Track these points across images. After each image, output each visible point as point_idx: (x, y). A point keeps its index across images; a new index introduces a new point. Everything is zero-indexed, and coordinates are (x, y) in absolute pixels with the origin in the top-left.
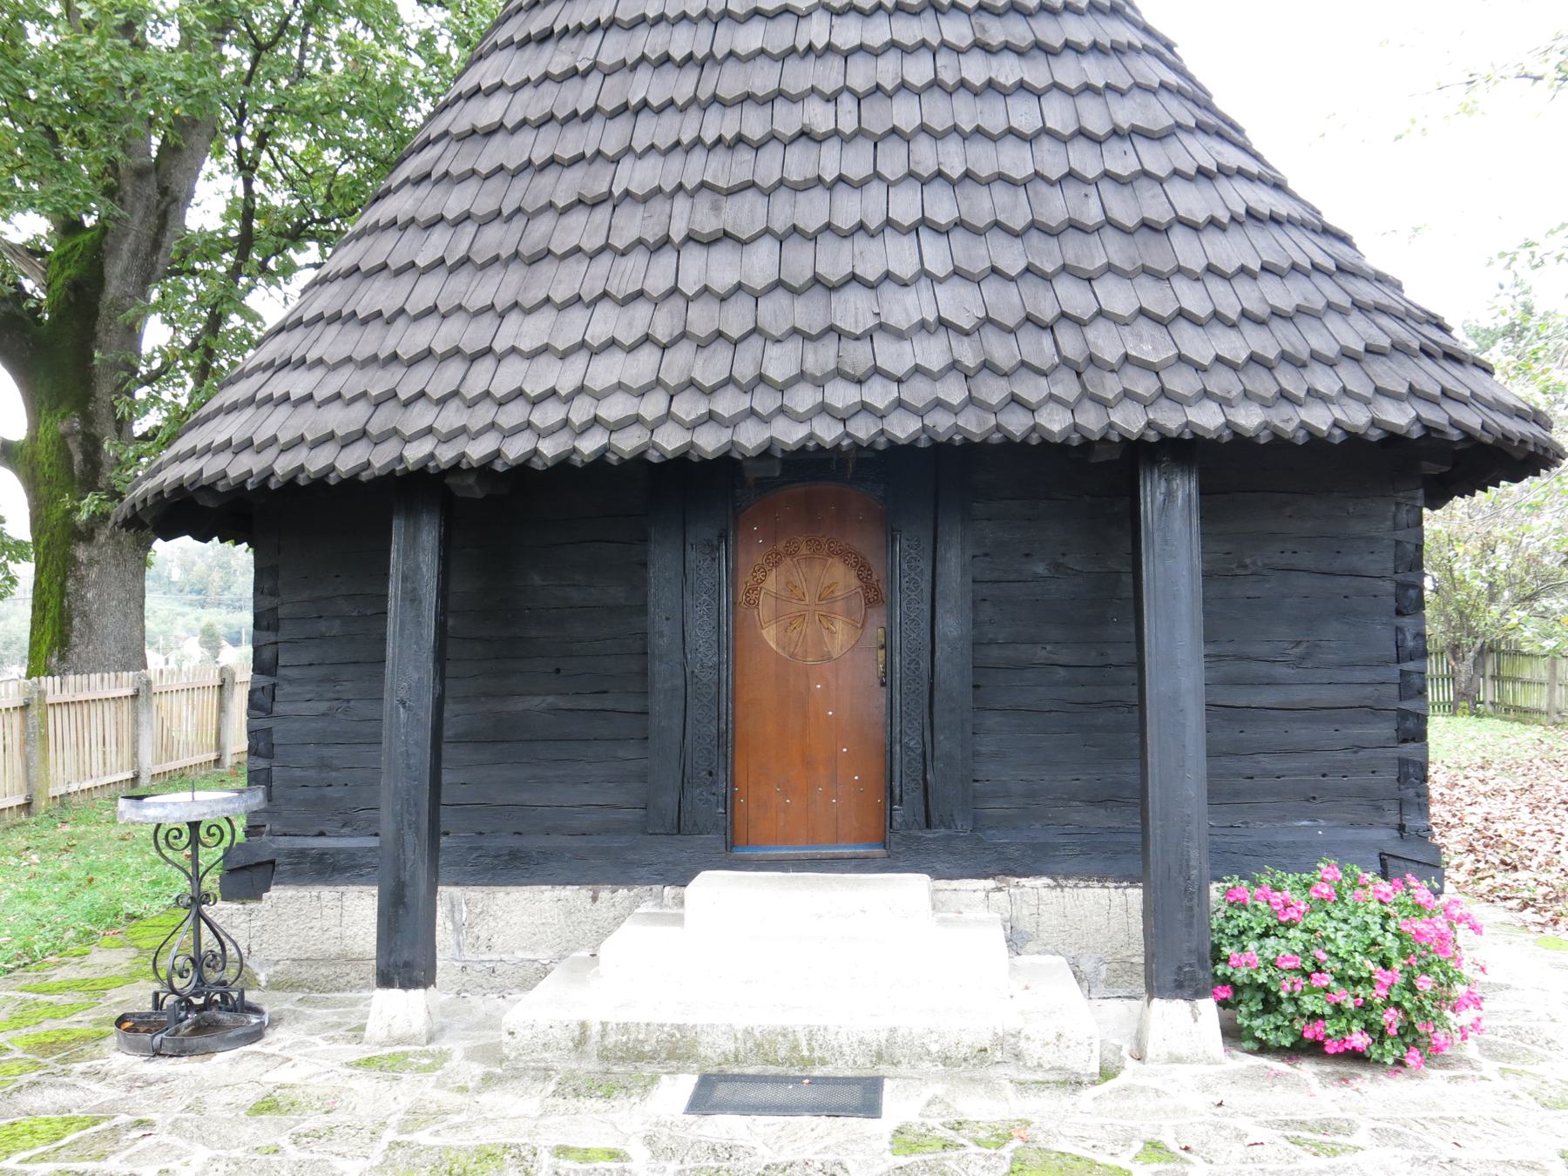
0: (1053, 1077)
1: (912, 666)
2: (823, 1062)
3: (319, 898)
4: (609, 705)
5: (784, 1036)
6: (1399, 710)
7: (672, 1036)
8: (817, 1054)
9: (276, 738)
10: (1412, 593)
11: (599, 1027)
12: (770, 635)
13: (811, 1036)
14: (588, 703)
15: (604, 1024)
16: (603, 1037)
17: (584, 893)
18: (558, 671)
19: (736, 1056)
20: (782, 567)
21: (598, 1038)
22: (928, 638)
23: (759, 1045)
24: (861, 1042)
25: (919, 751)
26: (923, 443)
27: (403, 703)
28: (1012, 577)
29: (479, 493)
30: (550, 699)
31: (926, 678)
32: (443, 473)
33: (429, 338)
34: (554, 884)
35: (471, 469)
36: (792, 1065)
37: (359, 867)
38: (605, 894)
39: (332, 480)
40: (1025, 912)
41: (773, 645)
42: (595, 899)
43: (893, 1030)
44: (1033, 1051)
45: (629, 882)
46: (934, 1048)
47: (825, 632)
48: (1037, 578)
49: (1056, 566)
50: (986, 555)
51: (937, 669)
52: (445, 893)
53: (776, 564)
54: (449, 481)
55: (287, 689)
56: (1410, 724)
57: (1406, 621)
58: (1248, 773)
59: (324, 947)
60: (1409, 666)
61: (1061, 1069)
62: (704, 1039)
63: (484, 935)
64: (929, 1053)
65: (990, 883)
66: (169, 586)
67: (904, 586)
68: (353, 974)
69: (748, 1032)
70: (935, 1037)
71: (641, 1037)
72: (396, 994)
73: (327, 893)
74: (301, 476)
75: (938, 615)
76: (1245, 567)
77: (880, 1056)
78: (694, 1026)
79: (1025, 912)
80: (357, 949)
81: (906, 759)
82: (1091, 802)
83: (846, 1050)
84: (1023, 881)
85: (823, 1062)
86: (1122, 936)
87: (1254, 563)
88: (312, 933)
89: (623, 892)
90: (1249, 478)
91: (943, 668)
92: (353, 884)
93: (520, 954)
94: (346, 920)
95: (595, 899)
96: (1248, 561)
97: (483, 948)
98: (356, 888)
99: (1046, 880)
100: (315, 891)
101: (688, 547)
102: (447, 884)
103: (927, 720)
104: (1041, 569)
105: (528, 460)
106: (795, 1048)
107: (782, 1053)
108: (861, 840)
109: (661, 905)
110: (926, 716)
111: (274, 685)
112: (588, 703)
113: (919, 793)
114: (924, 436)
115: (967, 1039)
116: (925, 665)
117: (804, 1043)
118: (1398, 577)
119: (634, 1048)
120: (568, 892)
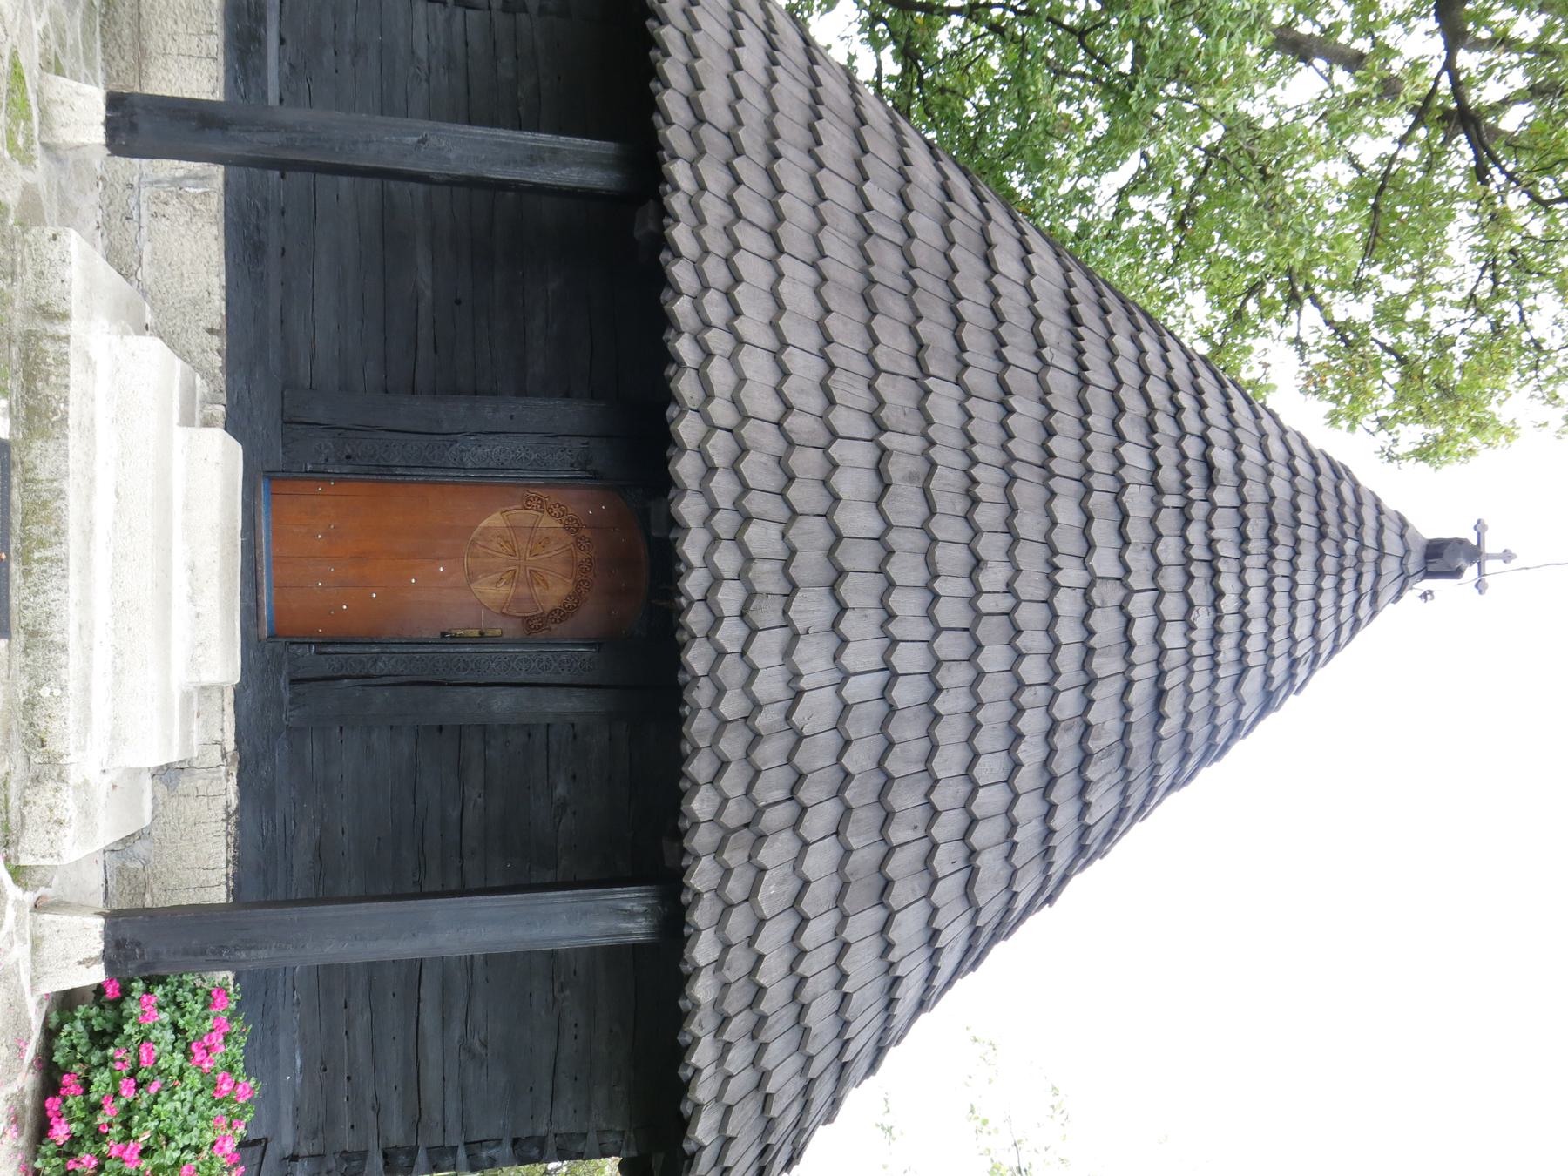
0: (14, 817)
2: (26, 574)
3: (211, 33)
5: (56, 533)
8: (36, 568)
10: (535, 1152)
11: (63, 332)
12: (495, 520)
16: (52, 337)
17: (218, 321)
18: (458, 302)
19: (31, 481)
20: (564, 534)
21: (50, 332)
23: (44, 505)
25: (372, 672)
27: (423, 141)
29: (638, 234)
30: (428, 293)
32: (659, 199)
33: (794, 191)
35: (662, 228)
36: (23, 540)
37: (246, 80)
38: (216, 342)
40: (200, 783)
41: (484, 523)
42: (211, 331)
43: (64, 648)
46: (45, 692)
51: (458, 689)
53: (567, 528)
57: (507, 1148)
58: (351, 1003)
59: (154, 35)
60: (462, 1155)
61: (23, 825)
63: (169, 210)
64: (39, 686)
65: (230, 746)
68: (123, 64)
69: (60, 494)
70: (57, 692)
71: (53, 379)
72: (99, 112)
73: (216, 43)
75: (513, 690)
76: (562, 990)
77: (34, 634)
78: (66, 436)
79: (200, 783)
80: (151, 70)
82: (319, 847)
84: (234, 780)
85: (26, 574)
86: (174, 882)
88: (170, 22)
89: (218, 361)
91: (459, 695)
92: (226, 72)
93: (147, 248)
94: (185, 61)
95: (211, 331)
96: (567, 993)
97: (154, 208)
99: (234, 803)
102: (226, 174)
103: (404, 679)
104: (560, 791)
106: (42, 544)
107: (36, 530)
109: (204, 401)
112: (424, 333)
113: (328, 672)
115: (55, 726)
116: (463, 677)
117: (48, 554)
118: (551, 1139)
119: (40, 371)
120: (218, 303)
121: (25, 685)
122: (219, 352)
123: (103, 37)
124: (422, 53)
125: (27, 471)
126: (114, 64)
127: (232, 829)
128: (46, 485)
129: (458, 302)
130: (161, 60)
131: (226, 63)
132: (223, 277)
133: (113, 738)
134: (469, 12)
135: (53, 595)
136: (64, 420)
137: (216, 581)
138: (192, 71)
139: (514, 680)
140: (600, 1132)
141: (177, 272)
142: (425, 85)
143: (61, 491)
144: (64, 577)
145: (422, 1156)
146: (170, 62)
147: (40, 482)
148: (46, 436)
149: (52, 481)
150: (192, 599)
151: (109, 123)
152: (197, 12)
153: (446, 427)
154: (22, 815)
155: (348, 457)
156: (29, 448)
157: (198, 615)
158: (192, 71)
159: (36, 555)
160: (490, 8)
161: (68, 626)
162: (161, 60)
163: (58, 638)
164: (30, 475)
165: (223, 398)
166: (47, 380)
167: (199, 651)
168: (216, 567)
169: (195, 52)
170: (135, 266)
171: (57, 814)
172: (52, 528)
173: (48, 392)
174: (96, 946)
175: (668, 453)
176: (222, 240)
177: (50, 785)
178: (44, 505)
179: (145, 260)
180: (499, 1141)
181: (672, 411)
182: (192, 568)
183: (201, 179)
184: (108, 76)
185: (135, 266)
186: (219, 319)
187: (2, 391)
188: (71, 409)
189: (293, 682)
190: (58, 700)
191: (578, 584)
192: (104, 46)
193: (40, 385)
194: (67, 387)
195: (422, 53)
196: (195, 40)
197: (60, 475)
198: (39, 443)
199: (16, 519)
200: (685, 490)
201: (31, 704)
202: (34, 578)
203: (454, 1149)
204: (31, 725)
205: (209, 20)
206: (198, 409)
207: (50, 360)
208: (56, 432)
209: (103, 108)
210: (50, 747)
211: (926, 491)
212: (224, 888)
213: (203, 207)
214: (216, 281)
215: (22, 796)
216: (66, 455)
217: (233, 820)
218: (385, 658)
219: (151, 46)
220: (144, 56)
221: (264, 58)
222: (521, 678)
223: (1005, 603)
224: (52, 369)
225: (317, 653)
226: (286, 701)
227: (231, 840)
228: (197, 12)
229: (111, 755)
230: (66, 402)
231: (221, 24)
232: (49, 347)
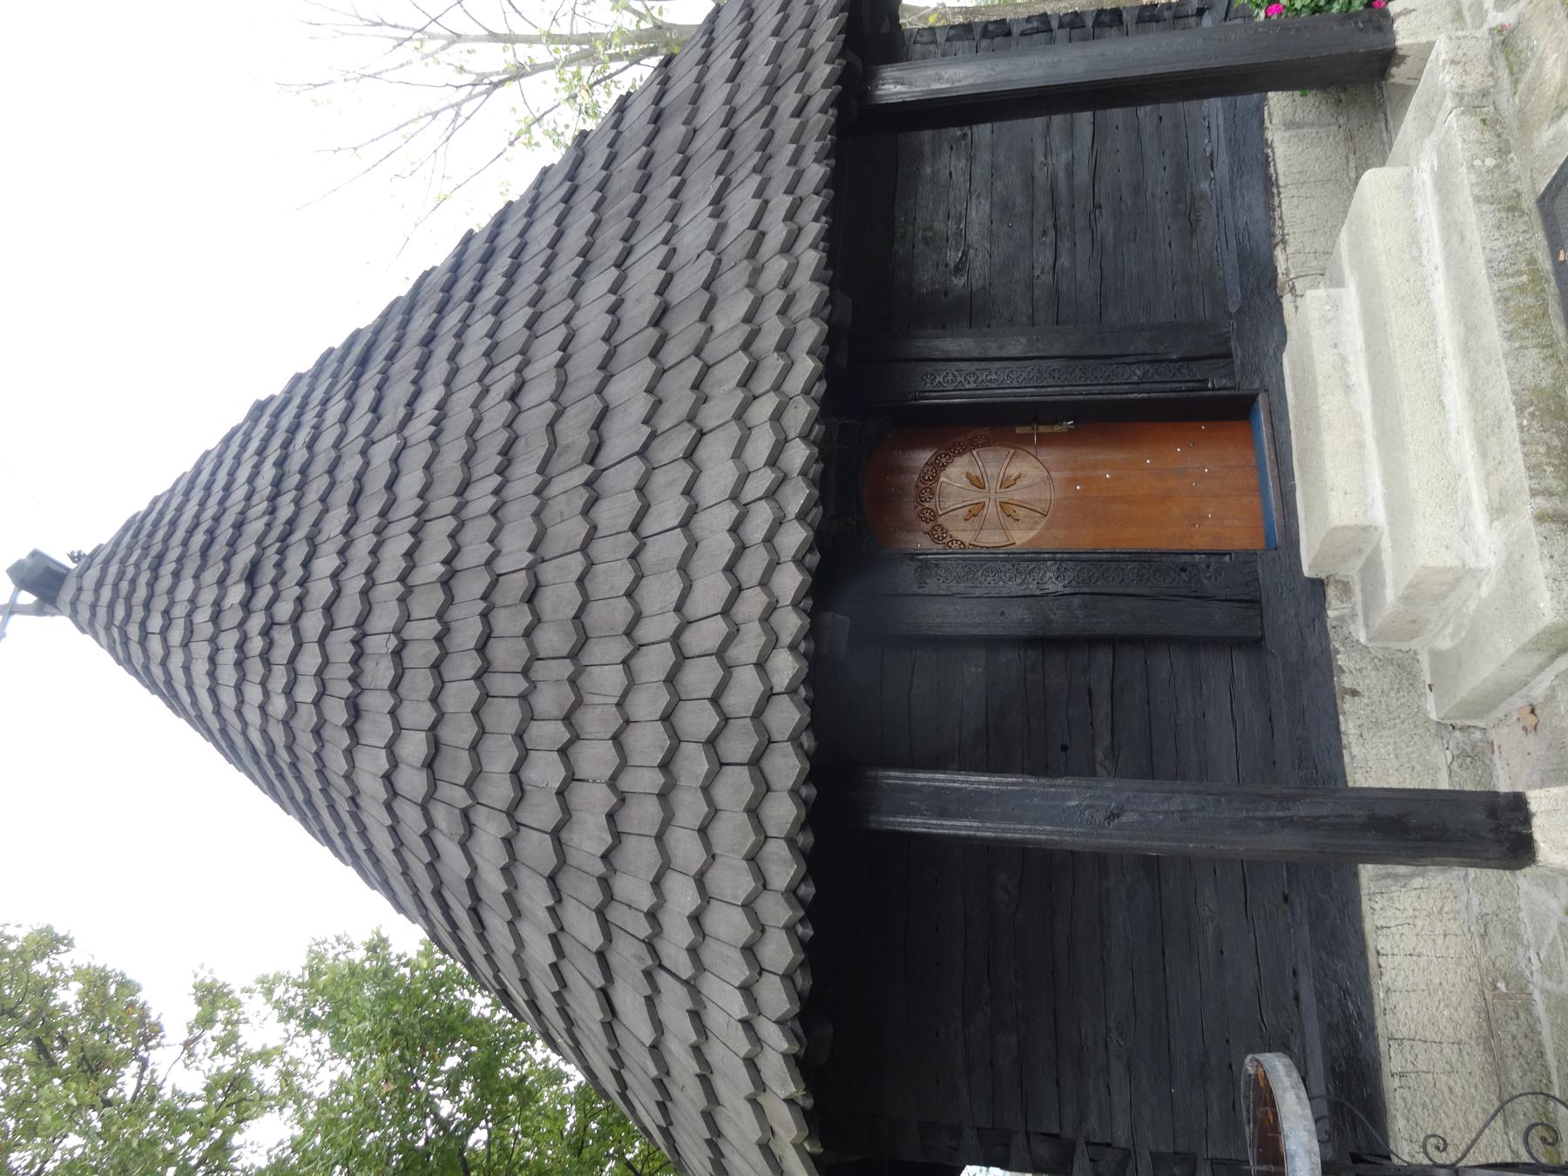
0: (1502, 63)
2: (1532, 261)
3: (1402, 1075)
4: (1105, 686)
5: (1507, 300)
6: (1093, 27)
7: (1532, 415)
8: (1523, 267)
9: (1165, 1147)
10: (991, 28)
11: (1539, 499)
13: (1501, 274)
14: (1103, 710)
15: (1534, 493)
16: (1551, 494)
17: (1347, 705)
18: (1064, 748)
19: (1546, 346)
20: (947, 525)
21: (1556, 500)
23: (1526, 324)
24: (1499, 227)
25: (1147, 366)
26: (803, 982)
27: (1113, 816)
30: (1100, 755)
31: (1070, 363)
36: (1543, 290)
37: (1347, 1018)
38: (1347, 681)
39: (807, 931)
40: (1314, 264)
41: (1032, 534)
42: (1354, 693)
43: (1477, 200)
44: (1473, 81)
46: (1490, 162)
53: (944, 530)
55: (1093, 1122)
56: (1106, 19)
57: (1016, 30)
58: (1156, 121)
59: (1478, 1073)
60: (1055, 24)
61: (1491, 58)
62: (1529, 380)
64: (1498, 166)
65: (1287, 301)
67: (973, 386)
68: (1513, 1028)
69: (1510, 336)
70: (1477, 163)
71: (1542, 450)
72: (1541, 830)
73: (1393, 1062)
74: (804, 792)
77: (1511, 209)
78: (1514, 392)
79: (1314, 264)
80: (1473, 1019)
81: (1156, 378)
82: (1193, 231)
83: (1511, 240)
84: (1280, 270)
85: (1532, 261)
86: (1330, 186)
88: (1458, 1090)
89: (1341, 660)
90: (875, 418)
91: (1057, 349)
92: (1373, 1028)
94: (1430, 1034)
95: (1354, 693)
99: (1278, 252)
100: (1391, 1084)
101: (926, 591)
103: (1115, 360)
105: (799, 994)
106: (1521, 289)
107: (1530, 300)
108: (1252, 441)
109: (1354, 615)
111: (1088, 1143)
112: (1103, 710)
114: (800, 929)
115: (1474, 135)
116: (1056, 364)
117: (1512, 281)
118: (977, 37)
119: (1559, 457)
120: (1349, 726)
121: (1511, 166)
123: (1544, 1066)
124: (1117, 1067)
125: (1552, 356)
126: (1524, 1028)
127: (1278, 231)
128: (1528, 343)
129: (1064, 748)
130: (1463, 1034)
131: (1376, 1038)
132: (1347, 759)
133: (1410, 189)
134: (1056, 1130)
135: (1498, 244)
136: (1520, 409)
137: (1320, 379)
139: (1003, 364)
140: (934, 42)
141: (1403, 760)
142: (1112, 1024)
143: (1509, 339)
144: (1490, 261)
145: (1089, 22)
146: (1449, 1032)
147: (1537, 346)
148: (1536, 390)
149: (1521, 347)
150: (1344, 360)
151: (1527, 818)
152: (1424, 1106)
153: (1076, 600)
154: (1492, 64)
155: (1184, 570)
156: (1555, 378)
157: (1335, 346)
159: (1525, 278)
160: (1027, 1134)
161: (1475, 223)
162: (1463, 1034)
163: (1485, 207)
164: (1550, 352)
166: (1549, 448)
167: (1330, 315)
168: (1320, 390)
169: (1419, 1048)
170: (1455, 766)
171: (1459, 69)
172: (1512, 303)
173: (1546, 436)
174: (1398, 25)
175: (827, 348)
177: (1470, 90)
178: (1526, 324)
180: (1023, 34)
181: (816, 469)
182: (1347, 388)
184: (1529, 1011)
185: (1455, 766)
186: (1346, 706)
187: (1560, 1005)
188: (1515, 422)
189: (1230, 356)
190: (1475, 157)
191: (936, 479)
192: (1541, 1054)
193: (1556, 442)
194: (1523, 443)
195: (1117, 1067)
196: (1421, 1066)
197: (1514, 355)
198: (1544, 384)
199: (1554, 308)
201: (1503, 152)
202: (1522, 258)
203: (1061, 26)
204: (1499, 136)
205: (1406, 1092)
206: (1359, 609)
207: (1549, 469)
208: (1527, 396)
209: (1537, 835)
210: (1476, 120)
211: (554, 443)
212: (1281, 183)
214: (1355, 751)
215: (1497, 80)
216: (1510, 374)
217: (1278, 238)
219: (1480, 1056)
220: (1486, 1041)
221: (1327, 1050)
223: (521, 685)
224: (1545, 460)
225: (1205, 381)
226: (1234, 338)
227: (1279, 223)
228: (1424, 1106)
229: (1410, 175)
230: (1521, 428)
231: (1388, 1096)
232: (1552, 483)
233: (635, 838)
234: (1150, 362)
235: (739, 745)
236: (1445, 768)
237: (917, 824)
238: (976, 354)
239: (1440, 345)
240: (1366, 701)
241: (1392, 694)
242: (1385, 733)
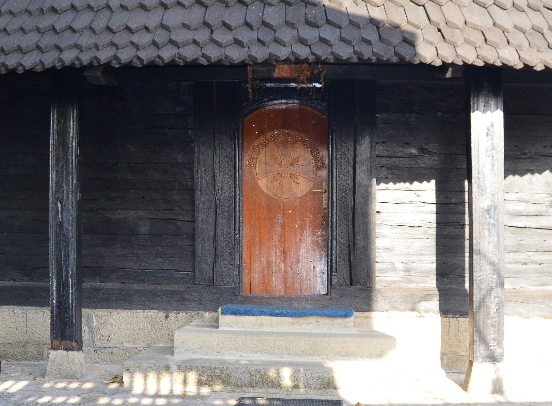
1: (343, 199)
12: (262, 183)
17: (162, 314)
22: (352, 185)
28: (399, 155)
29: (103, 81)
32: (84, 68)
33: (89, 21)
34: (144, 310)
35: (100, 65)
38: (172, 315)
42: (167, 317)
45: (186, 309)
47: (293, 183)
48: (411, 156)
49: (422, 150)
50: (384, 142)
51: (357, 201)
52: (85, 312)
53: (266, 146)
54: (86, 73)
58: (524, 261)
62: (233, 374)
63: (106, 334)
66: (435, 295)
67: (338, 156)
74: (20, 68)
75: (357, 173)
76: (525, 154)
87: (530, 152)
89: (182, 314)
93: (127, 345)
95: (167, 317)
96: (527, 151)
97: (106, 341)
98: (33, 308)
102: (85, 308)
104: (414, 151)
110: (351, 227)
113: (347, 267)
116: (350, 201)
120: (152, 313)
122: (177, 314)
138: (38, 321)
139: (351, 173)
141: (138, 331)
158: (38, 321)
165: (201, 313)
176: (119, 310)
179: (133, 346)
183: (89, 319)
186: (161, 313)
192: (26, 360)
200: (270, 53)
213: (103, 319)
218: (339, 239)
222: (351, 169)
233: (245, 11)
234: (349, 245)
235: (47, 40)
236: (135, 347)
237: (53, 124)
238: (358, 158)
239: (287, 356)
240: (164, 321)
241: (167, 332)
242: (149, 326)
